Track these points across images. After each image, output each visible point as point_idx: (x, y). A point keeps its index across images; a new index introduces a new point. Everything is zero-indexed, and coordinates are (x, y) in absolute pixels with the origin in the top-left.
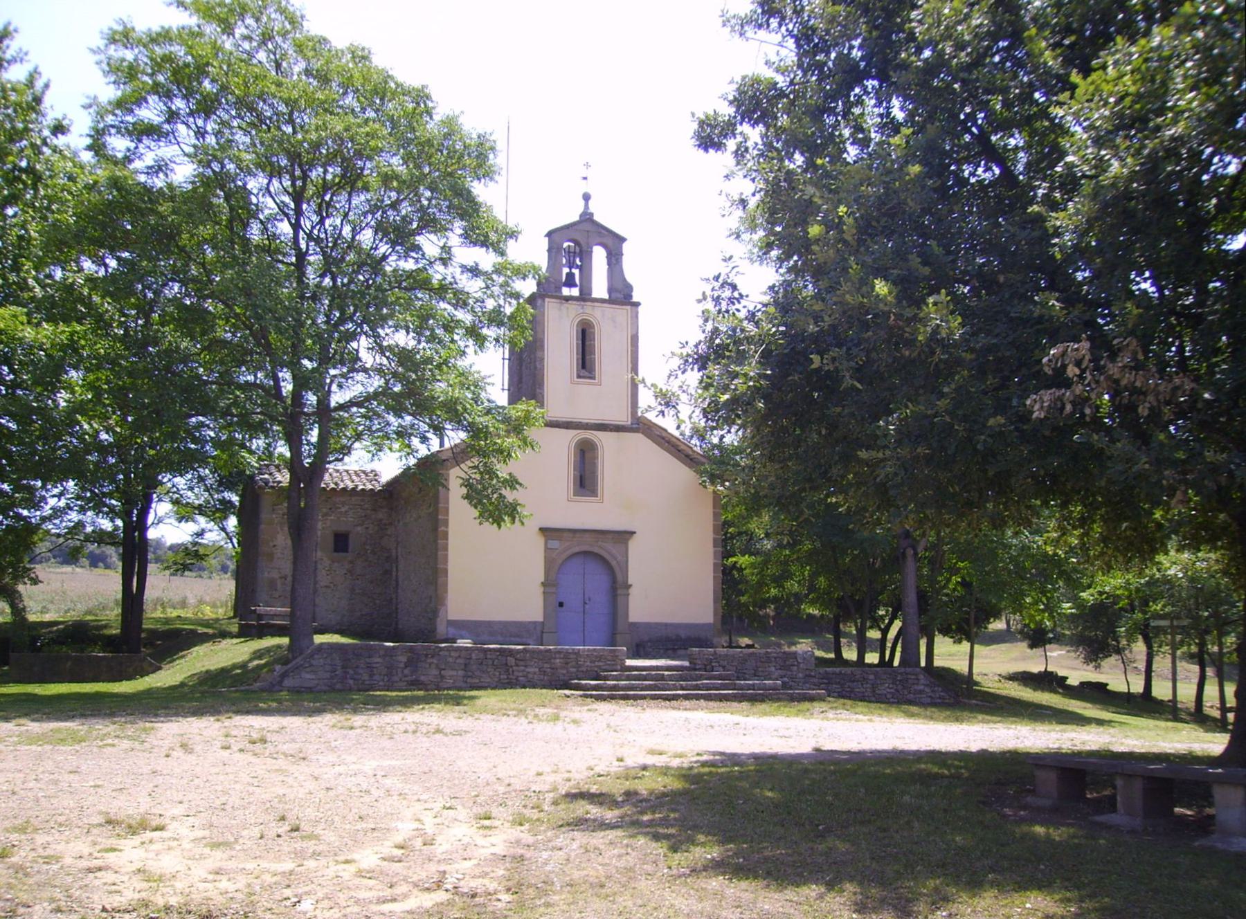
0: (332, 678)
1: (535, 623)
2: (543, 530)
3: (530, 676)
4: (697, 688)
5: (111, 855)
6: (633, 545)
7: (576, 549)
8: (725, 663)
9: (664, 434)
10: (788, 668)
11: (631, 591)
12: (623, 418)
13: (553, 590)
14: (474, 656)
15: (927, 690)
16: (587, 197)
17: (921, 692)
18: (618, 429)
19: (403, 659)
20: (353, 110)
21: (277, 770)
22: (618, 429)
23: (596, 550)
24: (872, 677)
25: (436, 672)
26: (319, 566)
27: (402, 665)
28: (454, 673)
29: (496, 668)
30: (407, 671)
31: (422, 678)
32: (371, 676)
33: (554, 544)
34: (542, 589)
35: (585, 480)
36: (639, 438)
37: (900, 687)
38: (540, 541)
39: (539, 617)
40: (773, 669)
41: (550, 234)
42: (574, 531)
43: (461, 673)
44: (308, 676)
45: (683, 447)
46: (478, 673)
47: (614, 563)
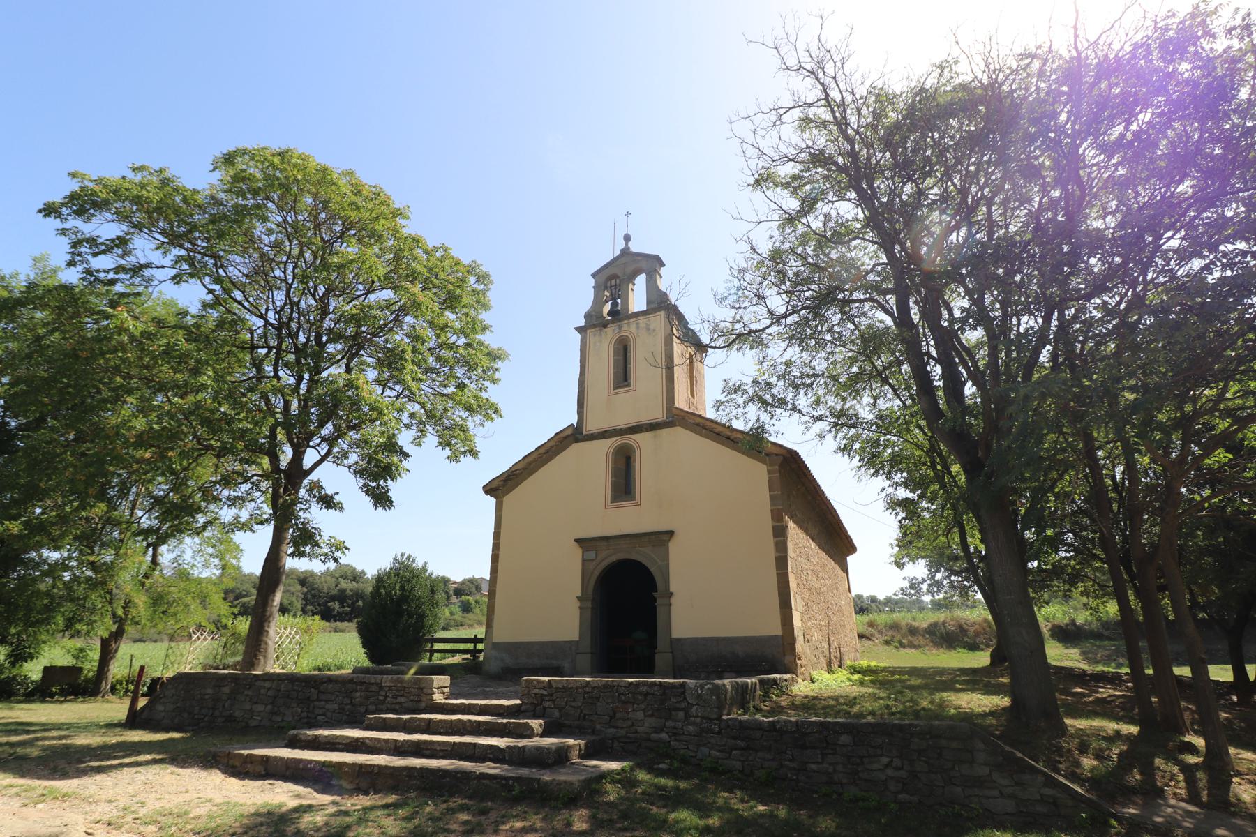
1: (570, 642)
2: (578, 541)
4: (429, 728)
6: (673, 546)
9: (698, 420)
11: (673, 600)
12: (658, 414)
16: (627, 238)
18: (653, 427)
20: (445, 386)
21: (822, 84)
22: (653, 427)
33: (591, 555)
34: (578, 604)
35: (623, 484)
36: (679, 430)
38: (578, 552)
39: (577, 639)
40: (640, 715)
41: (594, 275)
42: (607, 539)
45: (720, 429)
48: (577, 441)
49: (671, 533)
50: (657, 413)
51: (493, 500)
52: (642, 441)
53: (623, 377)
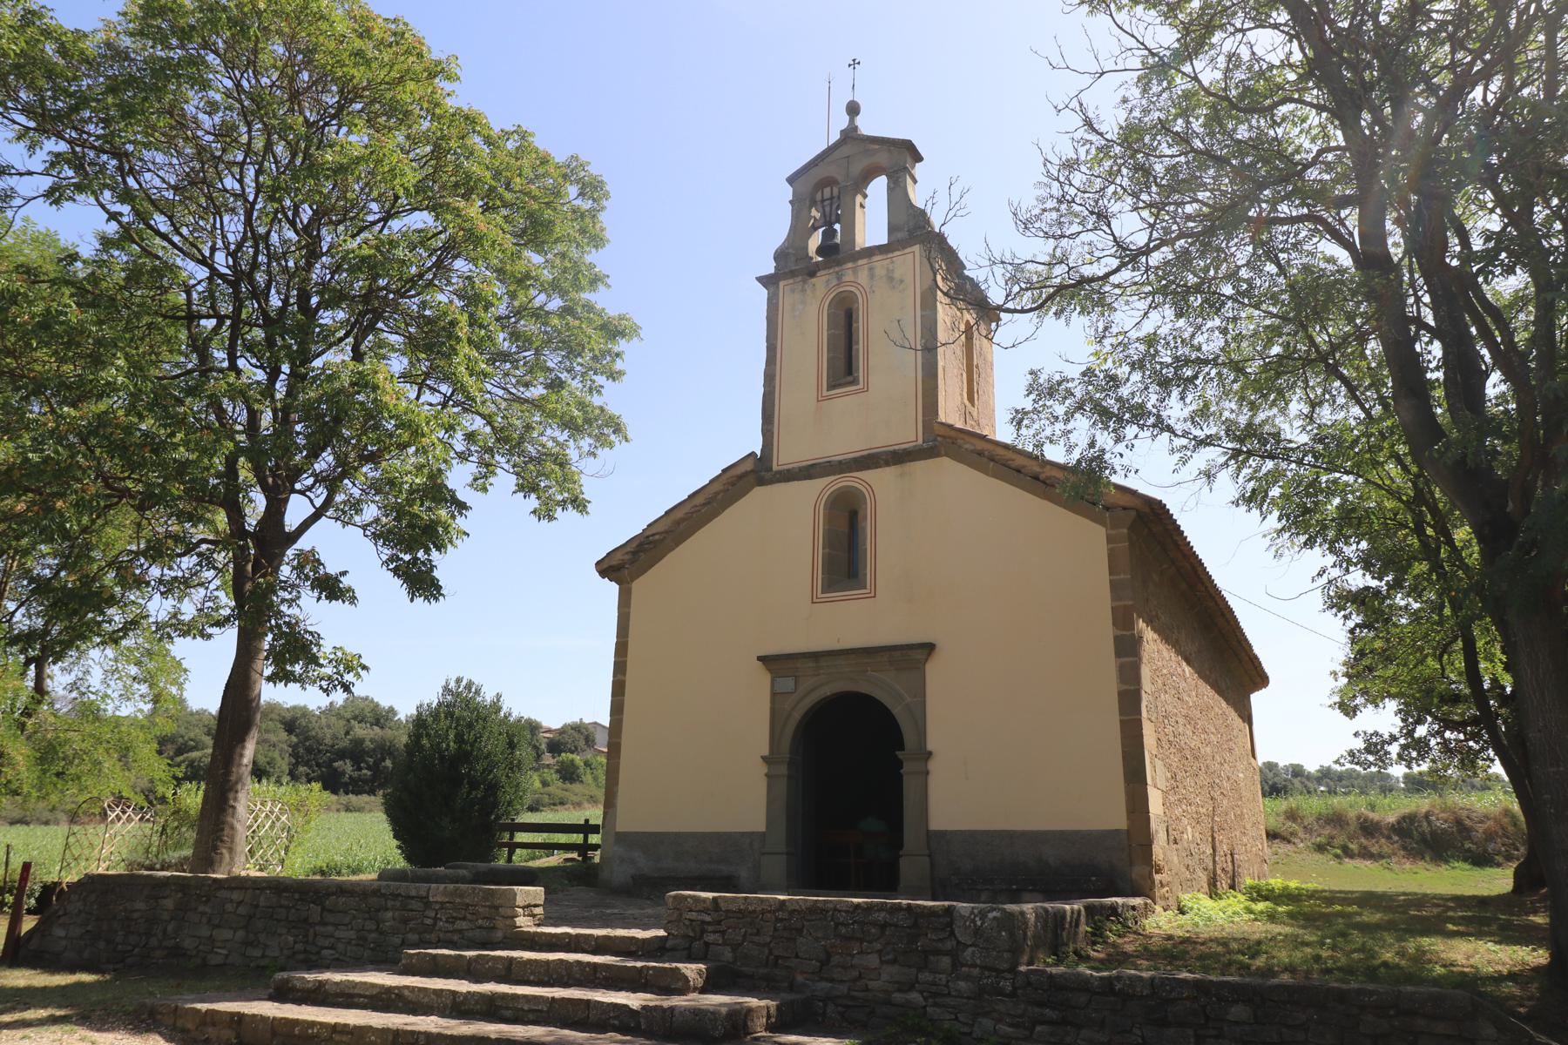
2: (760, 658)
6: (935, 671)
48: (762, 482)
49: (929, 648)
50: (908, 433)
51: (613, 588)
52: (880, 484)
53: (844, 367)
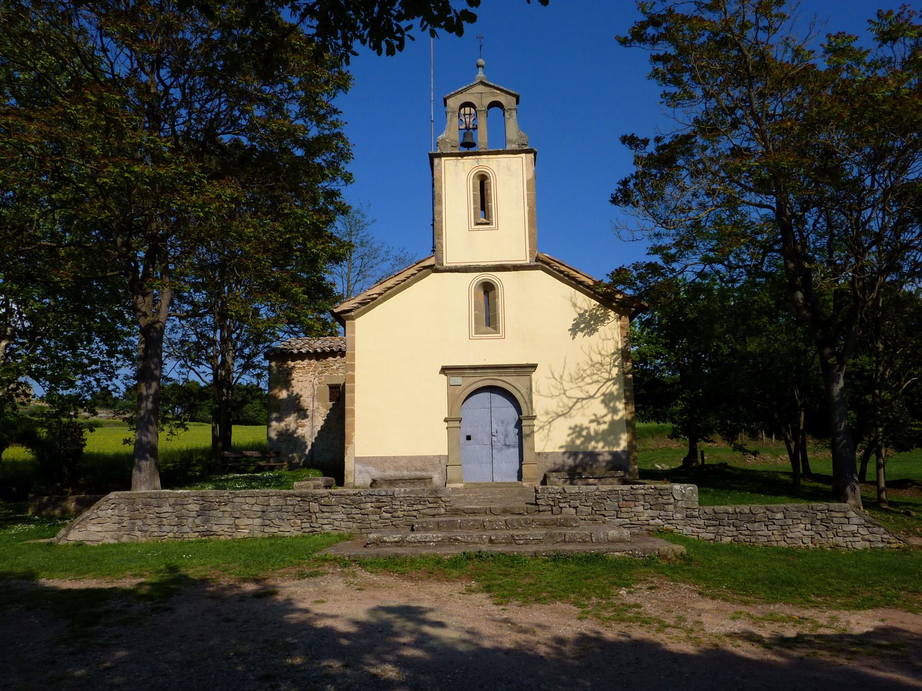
0: (119, 530)
1: (439, 456)
2: (445, 370)
3: (337, 523)
5: (320, 605)
7: (480, 385)
8: (577, 503)
10: (662, 507)
13: (457, 424)
14: (272, 502)
15: (863, 531)
17: (854, 534)
19: (194, 507)
23: (500, 384)
24: (779, 516)
25: (229, 521)
26: (316, 414)
27: (194, 514)
28: (250, 522)
29: (297, 515)
30: (198, 521)
31: (215, 528)
32: (160, 525)
33: (457, 380)
37: (821, 528)
40: (641, 509)
43: (258, 521)
44: (94, 528)
46: (277, 521)
47: (518, 396)
